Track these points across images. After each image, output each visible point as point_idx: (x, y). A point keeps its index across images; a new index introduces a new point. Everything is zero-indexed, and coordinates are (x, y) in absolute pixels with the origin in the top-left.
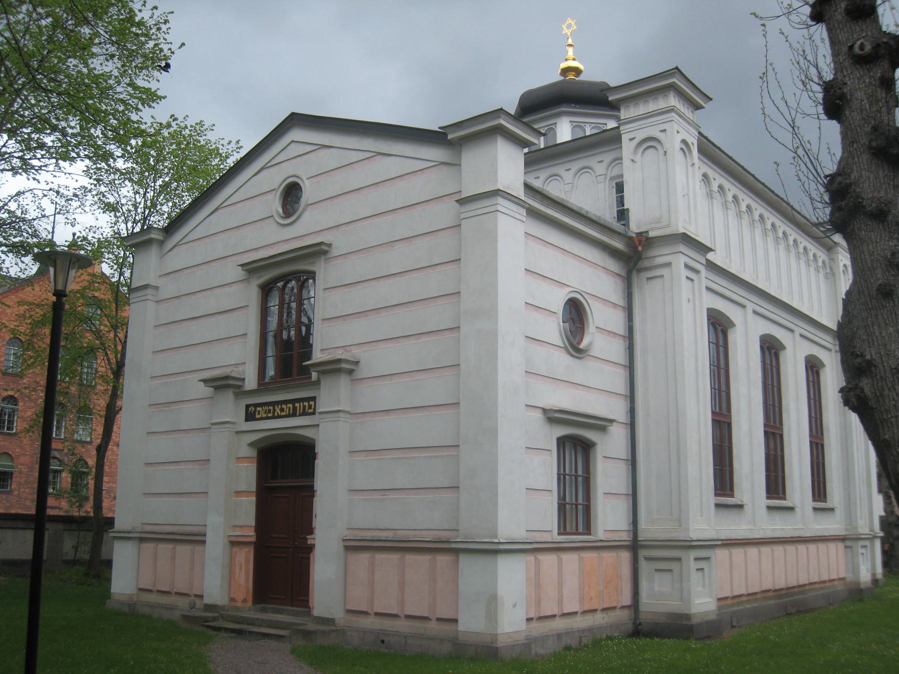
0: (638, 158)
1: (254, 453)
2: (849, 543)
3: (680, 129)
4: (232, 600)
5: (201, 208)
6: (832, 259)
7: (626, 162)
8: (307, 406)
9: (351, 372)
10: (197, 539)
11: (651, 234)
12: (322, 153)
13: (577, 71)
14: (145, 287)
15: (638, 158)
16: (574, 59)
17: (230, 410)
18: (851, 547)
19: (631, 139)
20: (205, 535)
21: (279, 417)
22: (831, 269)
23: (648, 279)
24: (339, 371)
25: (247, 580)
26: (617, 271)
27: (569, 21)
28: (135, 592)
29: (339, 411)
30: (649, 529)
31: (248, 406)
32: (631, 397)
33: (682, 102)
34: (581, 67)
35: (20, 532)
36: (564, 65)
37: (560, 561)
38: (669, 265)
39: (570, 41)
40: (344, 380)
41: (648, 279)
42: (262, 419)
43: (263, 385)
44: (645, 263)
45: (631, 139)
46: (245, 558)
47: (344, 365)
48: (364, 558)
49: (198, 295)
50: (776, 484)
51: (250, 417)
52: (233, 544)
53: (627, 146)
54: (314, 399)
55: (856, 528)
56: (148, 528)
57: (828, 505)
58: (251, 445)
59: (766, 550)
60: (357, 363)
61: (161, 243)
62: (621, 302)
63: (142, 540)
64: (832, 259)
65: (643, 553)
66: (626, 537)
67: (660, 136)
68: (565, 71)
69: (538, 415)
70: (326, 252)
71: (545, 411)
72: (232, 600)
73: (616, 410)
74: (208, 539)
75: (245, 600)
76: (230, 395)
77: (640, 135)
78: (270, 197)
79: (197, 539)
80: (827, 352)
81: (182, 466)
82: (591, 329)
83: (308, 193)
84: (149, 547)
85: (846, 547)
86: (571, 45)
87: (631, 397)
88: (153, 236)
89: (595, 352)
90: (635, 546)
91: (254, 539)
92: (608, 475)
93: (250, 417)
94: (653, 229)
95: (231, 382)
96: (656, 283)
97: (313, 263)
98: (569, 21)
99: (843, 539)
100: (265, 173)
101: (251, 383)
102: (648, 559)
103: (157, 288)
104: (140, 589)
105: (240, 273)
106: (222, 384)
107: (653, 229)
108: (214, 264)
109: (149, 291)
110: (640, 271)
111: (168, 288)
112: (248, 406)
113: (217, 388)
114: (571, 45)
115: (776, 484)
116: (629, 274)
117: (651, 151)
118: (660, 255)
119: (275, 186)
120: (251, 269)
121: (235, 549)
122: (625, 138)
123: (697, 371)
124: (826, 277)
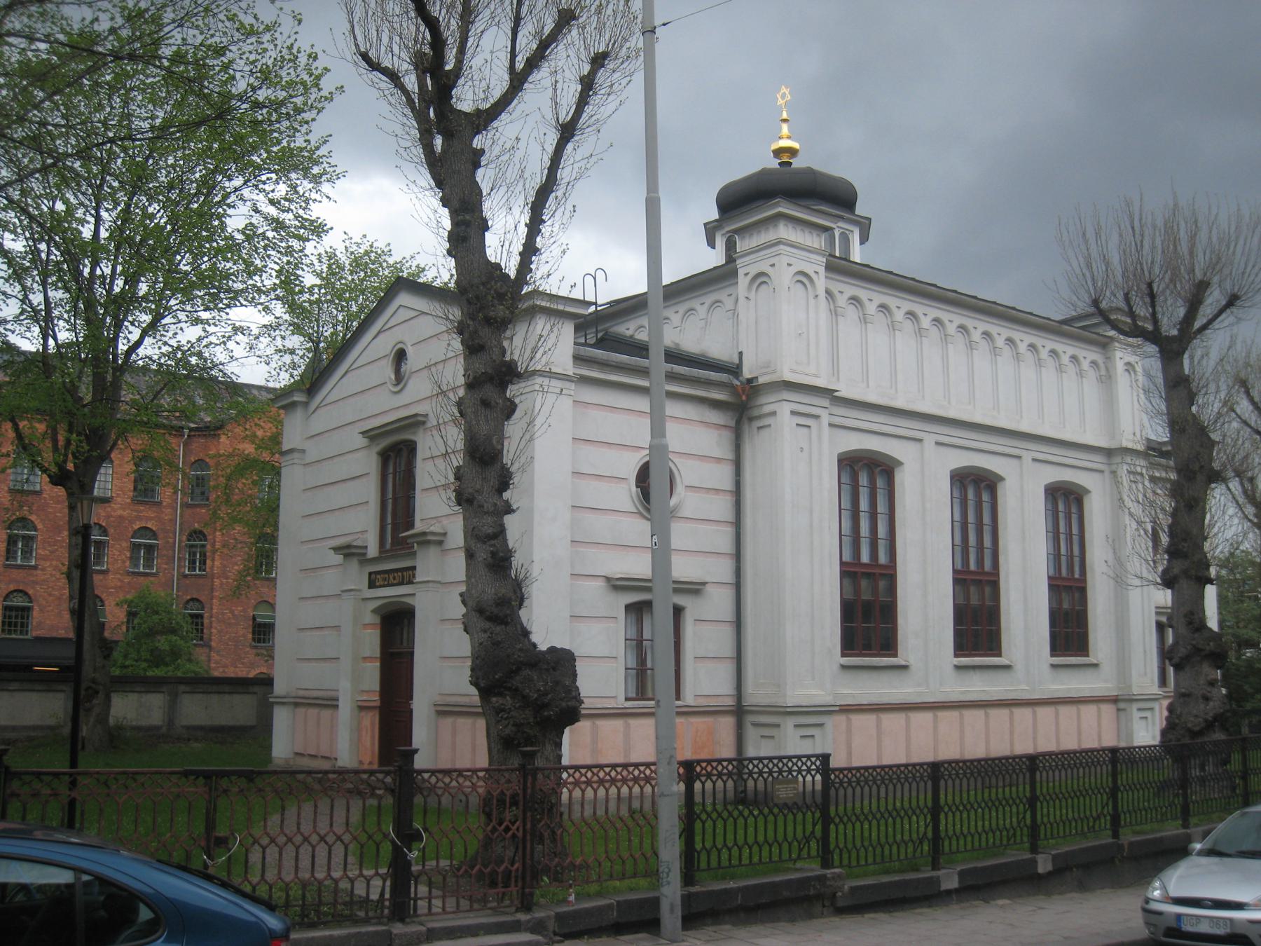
0: (752, 295)
1: (377, 620)
2: (1122, 705)
3: (792, 261)
4: (361, 762)
5: (335, 370)
6: (1108, 358)
7: (742, 300)
8: (406, 576)
9: (440, 543)
10: (330, 703)
11: (761, 380)
12: (423, 319)
13: (792, 152)
14: (291, 451)
15: (752, 295)
16: (789, 138)
17: (356, 577)
18: (1124, 710)
19: (746, 274)
20: (337, 700)
21: (393, 585)
22: (1107, 369)
23: (759, 428)
24: (428, 542)
25: (373, 744)
26: (722, 423)
27: (784, 90)
28: (292, 756)
29: (428, 582)
30: (755, 694)
31: (370, 574)
32: (738, 556)
33: (807, 231)
34: (796, 145)
35: (227, 696)
36: (774, 147)
37: (627, 727)
38: (774, 413)
39: (785, 116)
40: (433, 551)
41: (759, 428)
42: (381, 586)
43: (384, 554)
44: (755, 413)
45: (746, 274)
46: (371, 722)
47: (429, 538)
48: (449, 721)
49: (336, 460)
50: (977, 629)
51: (372, 585)
52: (361, 708)
53: (743, 281)
54: (414, 568)
55: (1130, 686)
56: (301, 693)
57: (1091, 659)
58: (375, 611)
59: (1063, 710)
60: (445, 534)
61: (306, 404)
62: (731, 456)
63: (296, 705)
64: (1108, 358)
65: (750, 719)
66: (730, 702)
67: (769, 271)
68: (778, 153)
69: (601, 583)
70: (424, 423)
71: (608, 579)
72: (361, 762)
73: (721, 571)
74: (341, 703)
75: (370, 763)
76: (354, 563)
77: (753, 271)
78: (384, 362)
79: (330, 703)
80: (1096, 476)
81: (326, 632)
82: (679, 488)
83: (414, 360)
84: (301, 710)
85: (1118, 710)
86: (785, 121)
87: (738, 556)
88: (295, 399)
89: (686, 512)
90: (740, 711)
91: (378, 704)
92: (704, 638)
93: (372, 585)
94: (763, 374)
95: (354, 551)
96: (764, 433)
97: (414, 433)
98: (784, 90)
99: (1115, 700)
100: (381, 337)
101: (373, 551)
102: (755, 725)
103: (303, 451)
104: (297, 754)
105: (362, 441)
106: (349, 552)
107: (763, 374)
108: (346, 428)
109: (296, 455)
110: (751, 419)
111: (313, 453)
112: (370, 574)
113: (346, 556)
114: (785, 121)
115: (977, 629)
116: (739, 422)
117: (764, 286)
118: (768, 403)
119: (388, 352)
120: (372, 436)
121: (363, 714)
122: (741, 272)
123: (811, 526)
124: (1100, 380)
